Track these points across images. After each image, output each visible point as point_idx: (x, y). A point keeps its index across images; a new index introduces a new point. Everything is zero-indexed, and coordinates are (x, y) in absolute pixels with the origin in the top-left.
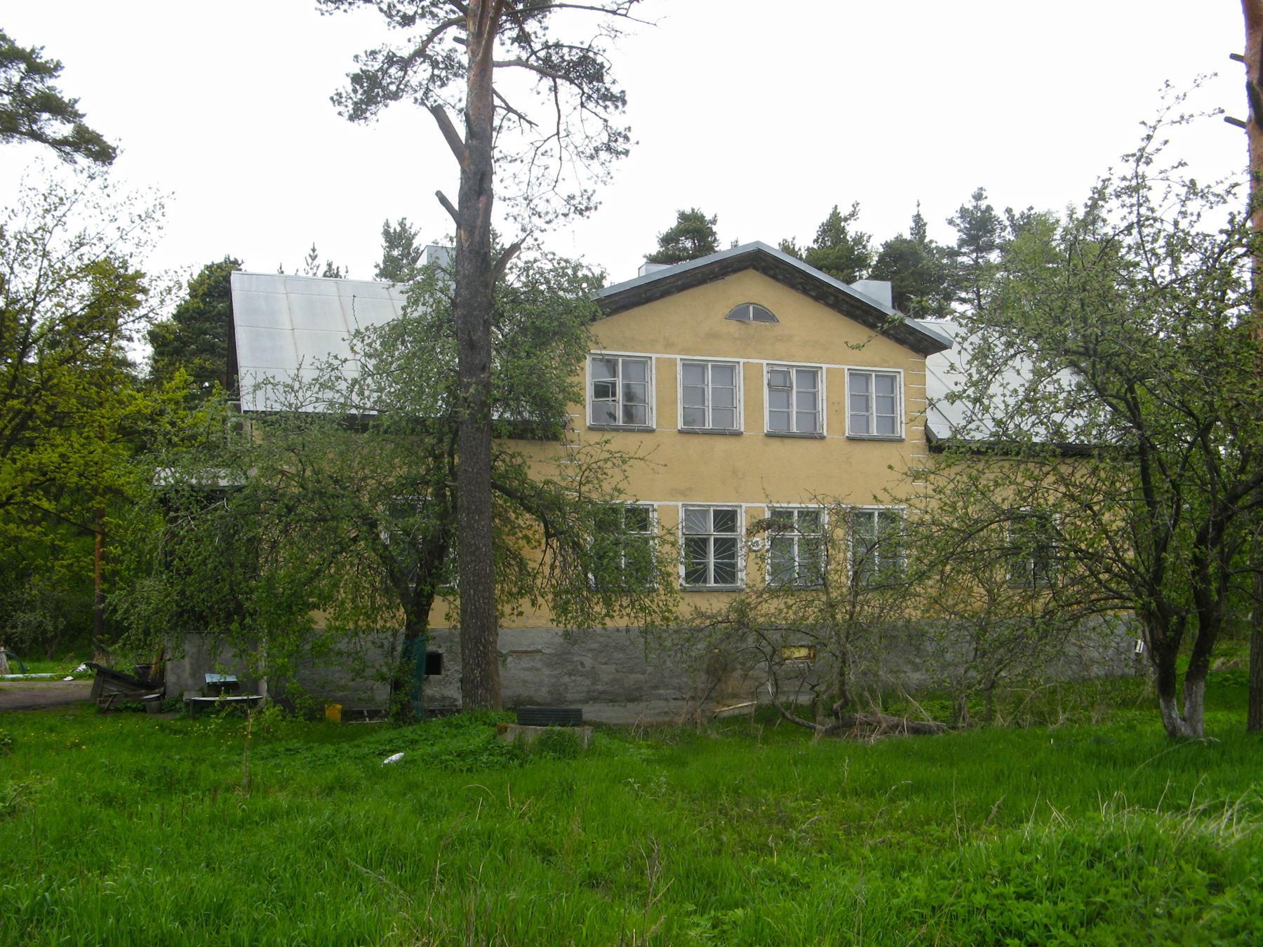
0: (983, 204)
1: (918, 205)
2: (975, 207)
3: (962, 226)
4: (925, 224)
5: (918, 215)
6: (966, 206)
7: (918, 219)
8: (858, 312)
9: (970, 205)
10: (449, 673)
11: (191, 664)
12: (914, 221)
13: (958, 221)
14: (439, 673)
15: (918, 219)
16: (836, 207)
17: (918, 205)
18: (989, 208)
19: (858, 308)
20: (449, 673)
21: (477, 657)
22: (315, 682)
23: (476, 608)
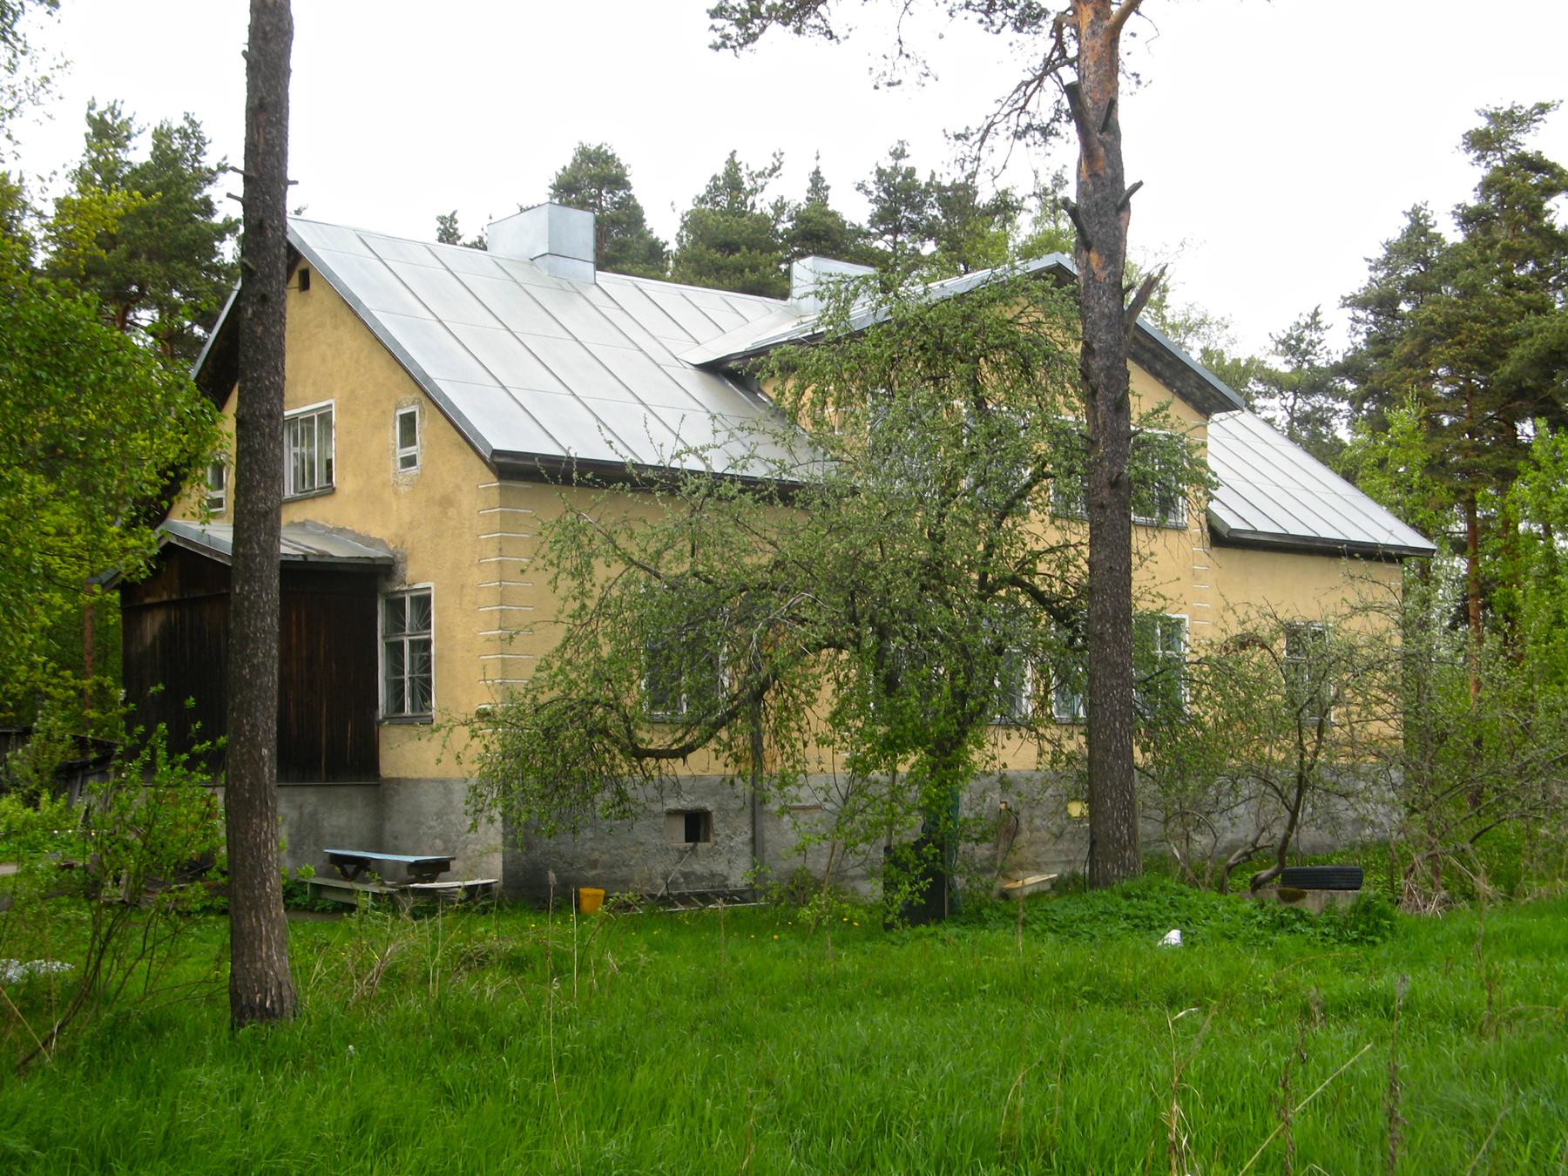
0: (904, 164)
1: (818, 158)
2: (895, 169)
3: (876, 193)
4: (827, 188)
5: (817, 173)
6: (883, 167)
7: (817, 177)
8: (1147, 356)
9: (887, 164)
10: (719, 839)
11: (290, 835)
12: (811, 180)
13: (872, 187)
14: (707, 840)
15: (817, 177)
16: (733, 154)
17: (818, 158)
18: (911, 172)
19: (1149, 350)
20: (719, 839)
21: (1124, 808)
22: (561, 857)
23: (1122, 746)
